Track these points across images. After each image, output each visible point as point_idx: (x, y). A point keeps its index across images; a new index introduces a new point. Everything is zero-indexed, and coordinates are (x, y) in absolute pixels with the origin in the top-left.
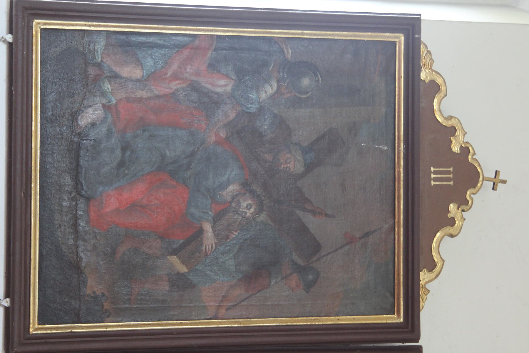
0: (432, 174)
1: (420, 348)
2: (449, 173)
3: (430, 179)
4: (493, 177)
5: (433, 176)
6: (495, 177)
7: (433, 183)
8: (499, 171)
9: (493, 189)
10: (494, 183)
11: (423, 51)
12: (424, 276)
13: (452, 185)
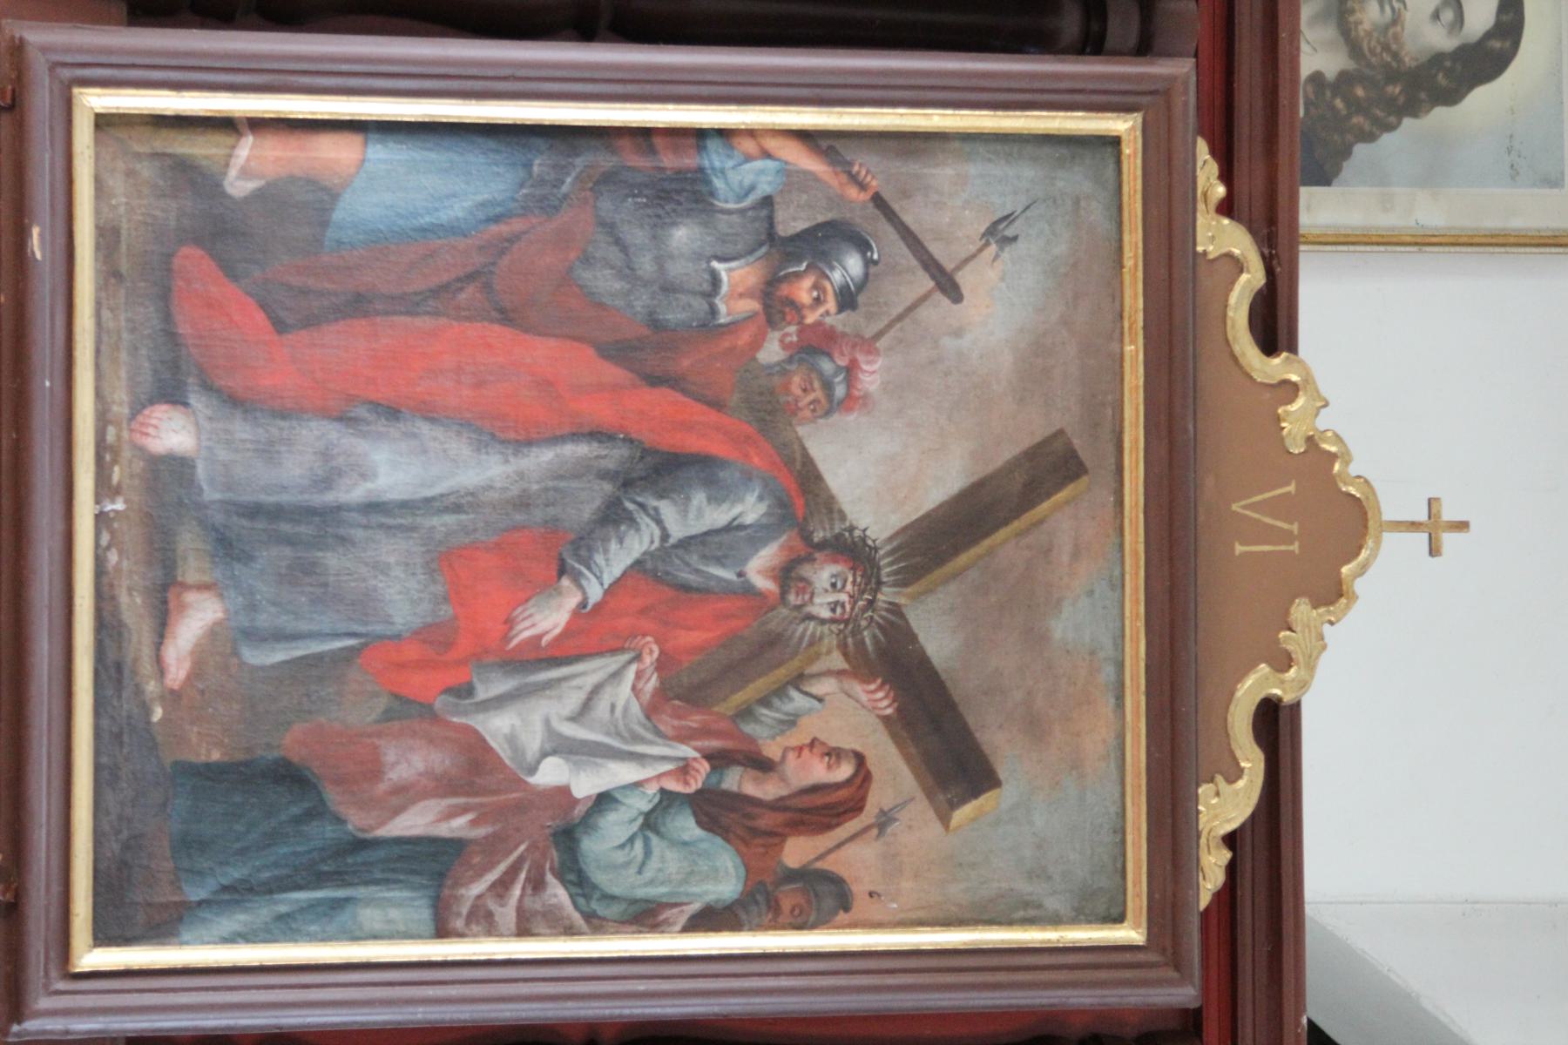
2: (1287, 537)
8: (1437, 499)
10: (1430, 535)
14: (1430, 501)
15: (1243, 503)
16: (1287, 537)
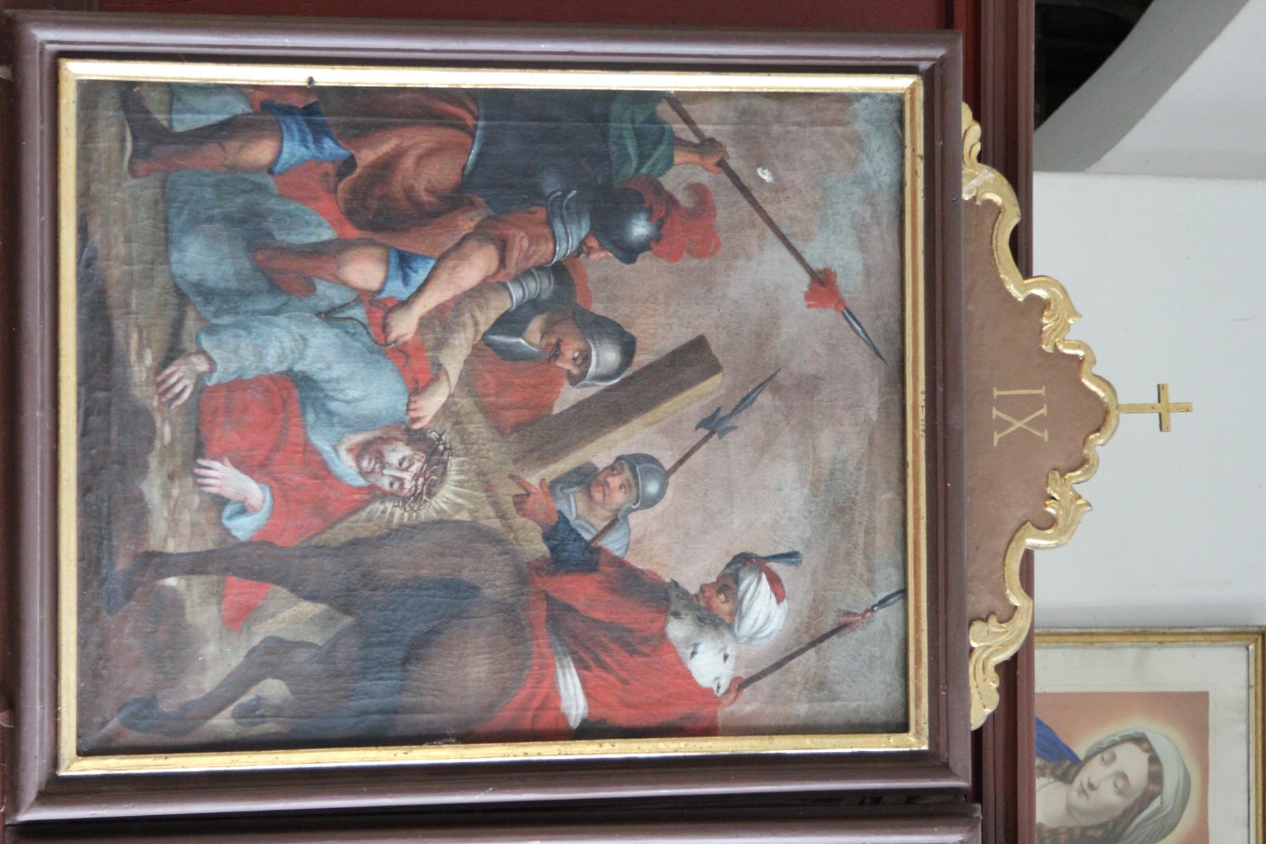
6: (1159, 401)
16: (1036, 402)
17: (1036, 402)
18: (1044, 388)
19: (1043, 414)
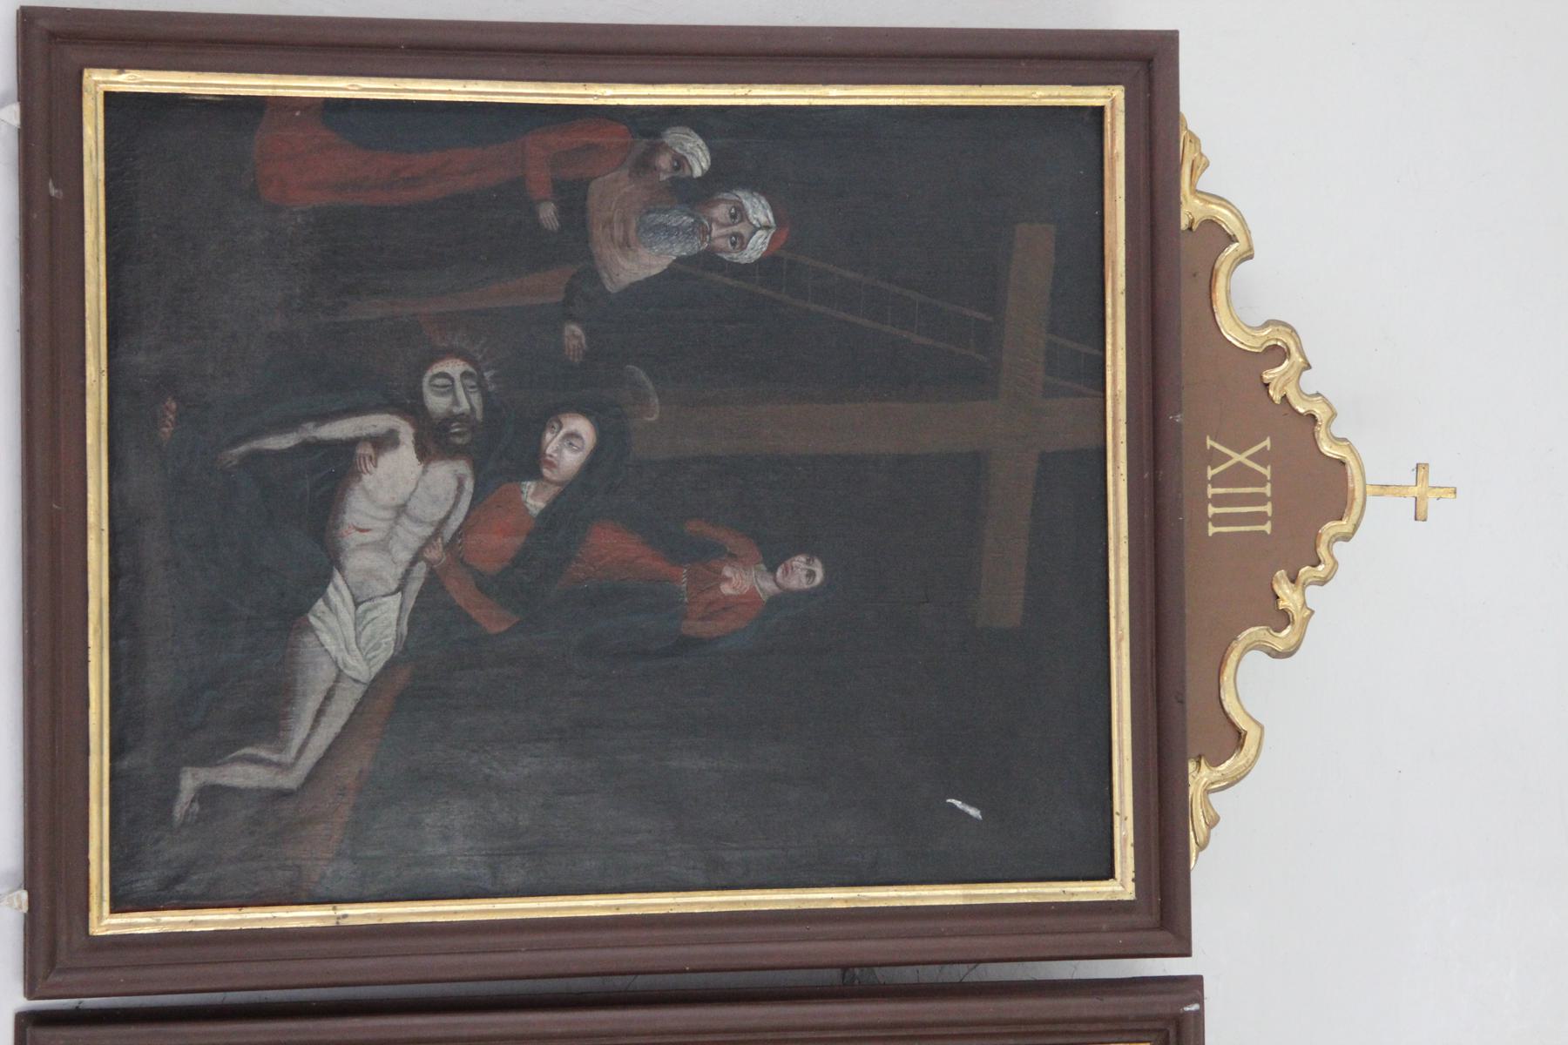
0: (1210, 506)
1: (1192, 986)
3: (1205, 519)
4: (1430, 484)
5: (1211, 491)
7: (1212, 530)
9: (1416, 519)
11: (1188, 155)
12: (1199, 777)
13: (1269, 532)
14: (1417, 465)
15: (1230, 463)
17: (1217, 481)
18: (1210, 534)
19: (1265, 447)
